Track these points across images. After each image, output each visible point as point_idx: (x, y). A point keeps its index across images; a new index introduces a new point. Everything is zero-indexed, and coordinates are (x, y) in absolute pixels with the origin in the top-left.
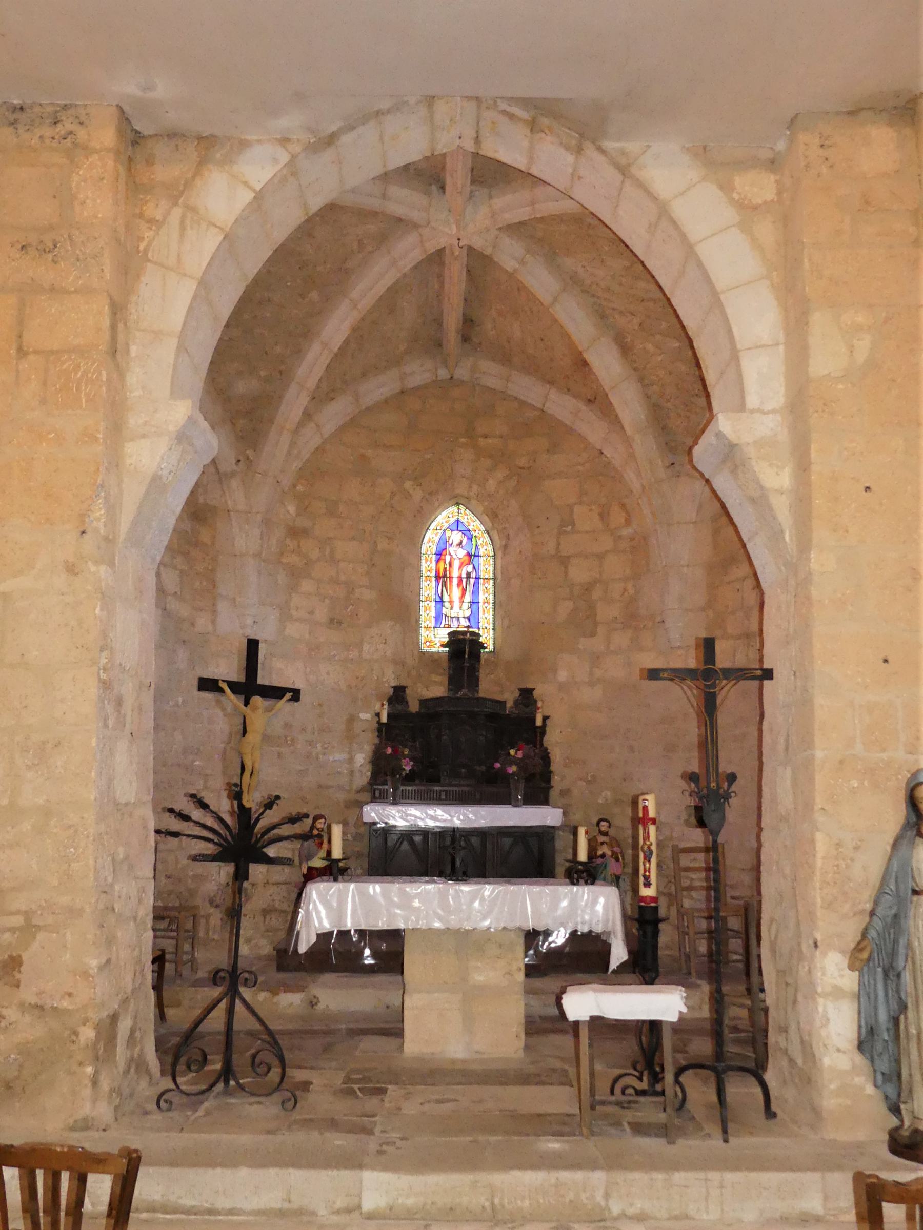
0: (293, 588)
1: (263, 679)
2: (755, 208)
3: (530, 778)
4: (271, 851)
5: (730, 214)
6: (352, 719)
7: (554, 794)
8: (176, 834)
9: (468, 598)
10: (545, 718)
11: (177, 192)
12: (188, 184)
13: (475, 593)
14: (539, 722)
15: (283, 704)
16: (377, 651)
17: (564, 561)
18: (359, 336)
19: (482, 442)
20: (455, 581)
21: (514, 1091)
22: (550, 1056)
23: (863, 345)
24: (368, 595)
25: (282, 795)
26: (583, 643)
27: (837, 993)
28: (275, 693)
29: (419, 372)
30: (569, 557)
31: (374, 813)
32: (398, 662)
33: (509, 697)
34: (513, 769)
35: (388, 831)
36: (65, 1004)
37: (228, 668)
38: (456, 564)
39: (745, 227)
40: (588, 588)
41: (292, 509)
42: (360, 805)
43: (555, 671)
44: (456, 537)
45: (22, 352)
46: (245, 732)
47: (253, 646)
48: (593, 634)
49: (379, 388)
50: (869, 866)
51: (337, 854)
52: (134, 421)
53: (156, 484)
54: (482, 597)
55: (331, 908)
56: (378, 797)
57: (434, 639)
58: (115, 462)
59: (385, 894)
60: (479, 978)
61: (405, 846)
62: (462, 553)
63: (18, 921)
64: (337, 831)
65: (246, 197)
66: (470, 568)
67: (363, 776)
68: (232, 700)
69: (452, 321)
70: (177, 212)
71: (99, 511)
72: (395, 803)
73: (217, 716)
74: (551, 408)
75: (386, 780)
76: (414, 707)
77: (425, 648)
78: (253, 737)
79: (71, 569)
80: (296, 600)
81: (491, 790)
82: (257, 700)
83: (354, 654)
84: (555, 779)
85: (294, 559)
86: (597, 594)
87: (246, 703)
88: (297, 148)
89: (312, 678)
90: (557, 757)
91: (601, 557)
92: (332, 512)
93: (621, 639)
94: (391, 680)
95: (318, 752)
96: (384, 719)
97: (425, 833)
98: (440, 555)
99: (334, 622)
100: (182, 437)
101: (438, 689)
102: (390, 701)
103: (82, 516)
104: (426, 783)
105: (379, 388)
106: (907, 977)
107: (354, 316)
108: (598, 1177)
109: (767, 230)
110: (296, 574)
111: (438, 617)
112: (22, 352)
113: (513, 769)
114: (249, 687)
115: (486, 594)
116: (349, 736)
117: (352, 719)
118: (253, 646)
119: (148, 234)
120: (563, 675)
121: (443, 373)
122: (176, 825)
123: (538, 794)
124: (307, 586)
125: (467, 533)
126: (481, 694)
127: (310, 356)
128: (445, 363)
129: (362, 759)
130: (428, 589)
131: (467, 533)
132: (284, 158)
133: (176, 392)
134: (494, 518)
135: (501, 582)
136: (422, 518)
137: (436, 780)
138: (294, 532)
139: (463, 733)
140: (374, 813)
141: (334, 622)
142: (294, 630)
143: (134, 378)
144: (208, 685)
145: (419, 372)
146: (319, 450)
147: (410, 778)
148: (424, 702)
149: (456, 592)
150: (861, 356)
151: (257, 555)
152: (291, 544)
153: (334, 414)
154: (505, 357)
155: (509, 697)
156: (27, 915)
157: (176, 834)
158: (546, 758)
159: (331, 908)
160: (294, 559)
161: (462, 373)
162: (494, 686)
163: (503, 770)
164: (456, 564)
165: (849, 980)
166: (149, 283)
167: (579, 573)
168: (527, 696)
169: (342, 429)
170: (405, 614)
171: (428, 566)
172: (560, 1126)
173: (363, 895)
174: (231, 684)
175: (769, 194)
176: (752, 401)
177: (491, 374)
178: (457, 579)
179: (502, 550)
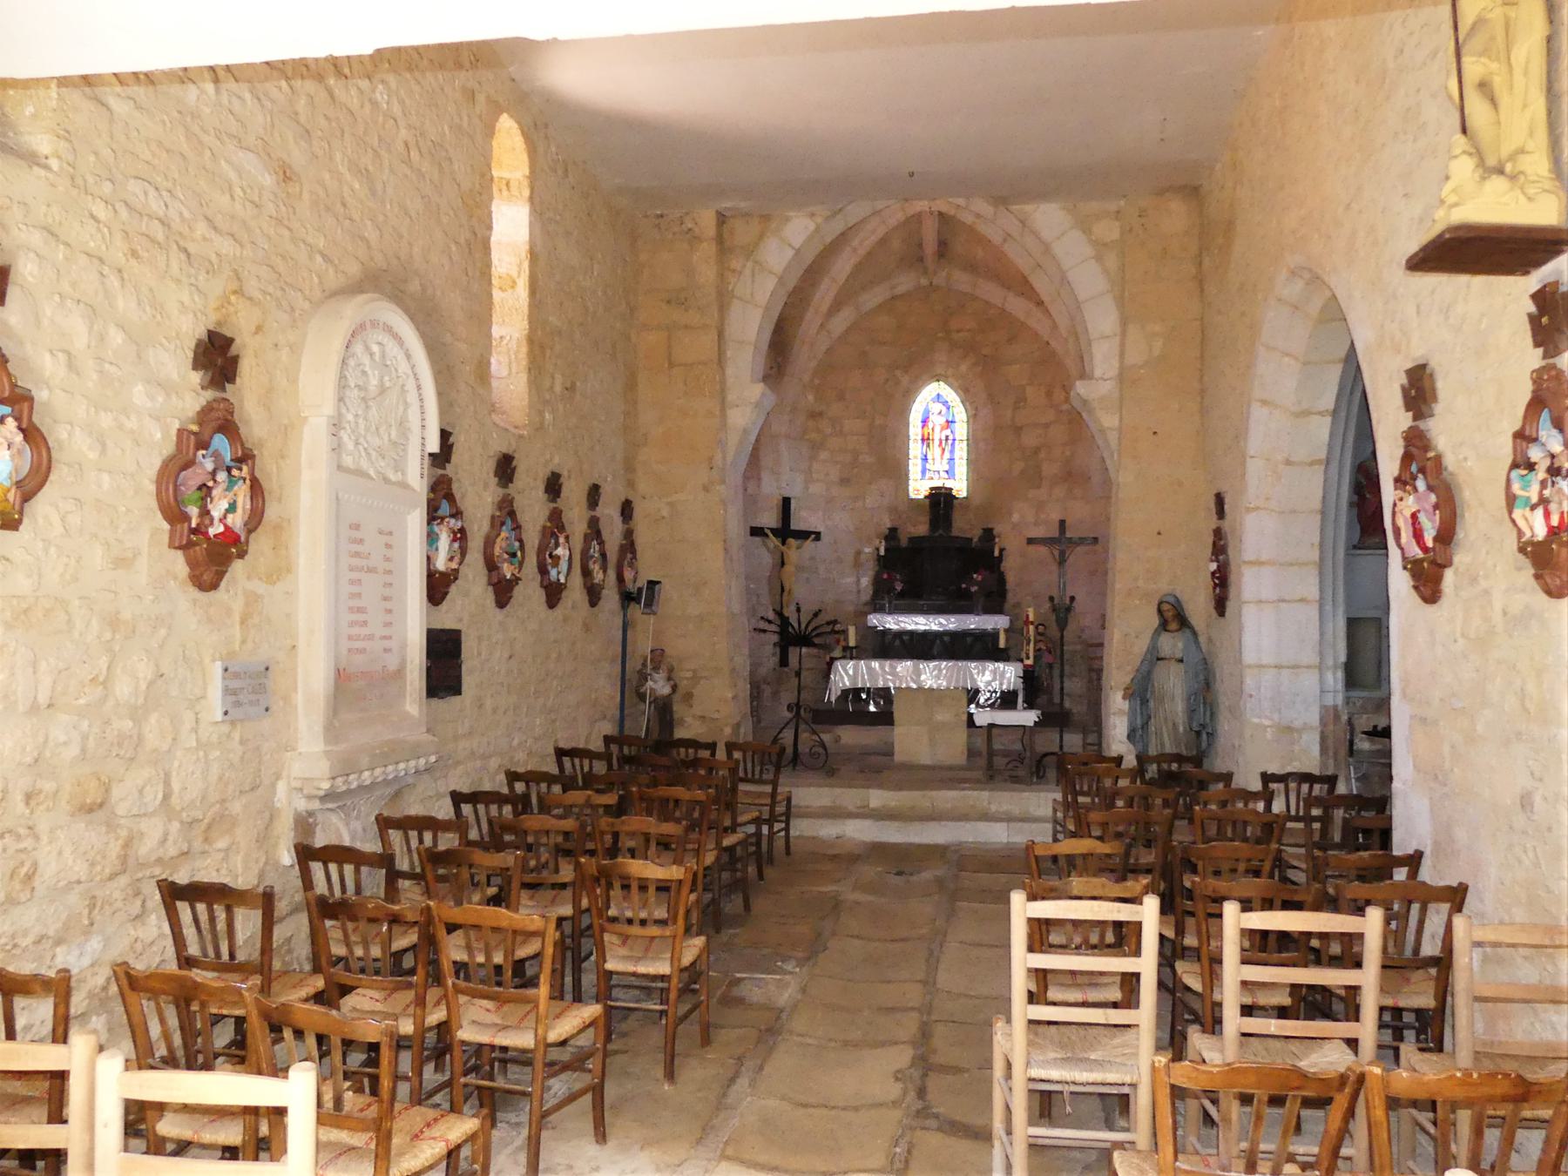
0: (813, 458)
1: (795, 525)
2: (1105, 245)
3: (989, 595)
4: (816, 641)
5: (1088, 251)
6: (859, 553)
7: (1007, 606)
8: (764, 631)
9: (947, 455)
10: (1002, 550)
11: (750, 251)
12: (756, 245)
13: (952, 452)
14: (996, 553)
15: (809, 544)
16: (875, 497)
17: (1018, 430)
18: (858, 268)
19: (955, 336)
20: (937, 442)
21: (1112, 1012)
22: (1195, 993)
23: (1158, 345)
24: (868, 459)
25: (192, 330)
26: (1032, 493)
27: (1121, 712)
28: (803, 535)
29: (905, 282)
30: (1021, 428)
31: (875, 620)
32: (893, 510)
33: (975, 534)
34: (974, 589)
35: (886, 632)
36: (716, 716)
37: (770, 519)
38: (937, 429)
39: (1099, 258)
40: (1037, 451)
41: (811, 397)
42: (866, 614)
43: (1011, 515)
44: (939, 407)
45: (671, 365)
46: (783, 564)
47: (786, 502)
48: (1039, 487)
49: (874, 298)
50: (1141, 646)
51: (852, 643)
52: (731, 397)
53: (745, 431)
54: (957, 455)
55: (847, 674)
56: (879, 609)
57: (919, 488)
58: (724, 425)
59: (882, 668)
60: (939, 717)
61: (897, 642)
62: (942, 420)
63: (689, 674)
64: (852, 631)
65: (790, 253)
66: (948, 432)
67: (866, 596)
68: (774, 541)
69: (930, 247)
70: (749, 264)
71: (719, 456)
72: (890, 613)
73: (764, 554)
74: (1008, 307)
75: (884, 597)
76: (904, 542)
77: (912, 495)
78: (788, 568)
79: (706, 489)
80: (815, 466)
81: (957, 603)
82: (791, 541)
83: (859, 504)
84: (1010, 596)
85: (814, 435)
86: (1042, 455)
87: (784, 543)
88: (819, 220)
89: (829, 523)
90: (1011, 579)
91: (1047, 426)
92: (841, 397)
93: (1059, 492)
94: (887, 523)
95: (836, 574)
96: (882, 552)
97: (912, 633)
98: (925, 422)
99: (844, 481)
100: (757, 405)
101: (921, 528)
102: (886, 538)
103: (711, 459)
104: (914, 599)
105: (874, 298)
106: (1151, 704)
107: (854, 260)
108: (985, 794)
109: (1112, 261)
110: (816, 447)
111: (924, 471)
112: (671, 365)
113: (974, 589)
114: (785, 532)
115: (961, 452)
116: (857, 564)
117: (859, 553)
118: (786, 502)
119: (733, 280)
120: (1016, 517)
121: (924, 282)
122: (763, 625)
123: (995, 608)
124: (823, 455)
125: (945, 403)
126: (955, 532)
127: (823, 287)
128: (925, 272)
129: (866, 581)
130: (915, 449)
131: (945, 403)
132: (812, 227)
133: (753, 381)
134: (966, 393)
135: (973, 442)
136: (909, 395)
137: (919, 597)
138: (814, 415)
139: (940, 559)
140: (875, 620)
141: (844, 481)
142: (815, 489)
143: (729, 371)
144: (756, 532)
145: (905, 282)
146: (829, 351)
147: (902, 595)
148: (911, 540)
149: (938, 451)
150: (1156, 352)
151: (788, 437)
152: (811, 423)
153: (840, 323)
154: (972, 267)
155: (975, 534)
156: (694, 671)
157: (764, 631)
158: (1002, 580)
159: (847, 674)
160: (814, 435)
161: (940, 279)
162: (964, 527)
163: (967, 589)
164: (937, 429)
165: (1125, 706)
166: (736, 309)
167: (1030, 439)
168: (989, 535)
169: (848, 331)
170: (898, 473)
171: (915, 430)
172: (978, 781)
173: (869, 668)
174: (772, 530)
175: (1115, 235)
176: (1098, 373)
177: (962, 280)
178: (940, 443)
179: (973, 418)
